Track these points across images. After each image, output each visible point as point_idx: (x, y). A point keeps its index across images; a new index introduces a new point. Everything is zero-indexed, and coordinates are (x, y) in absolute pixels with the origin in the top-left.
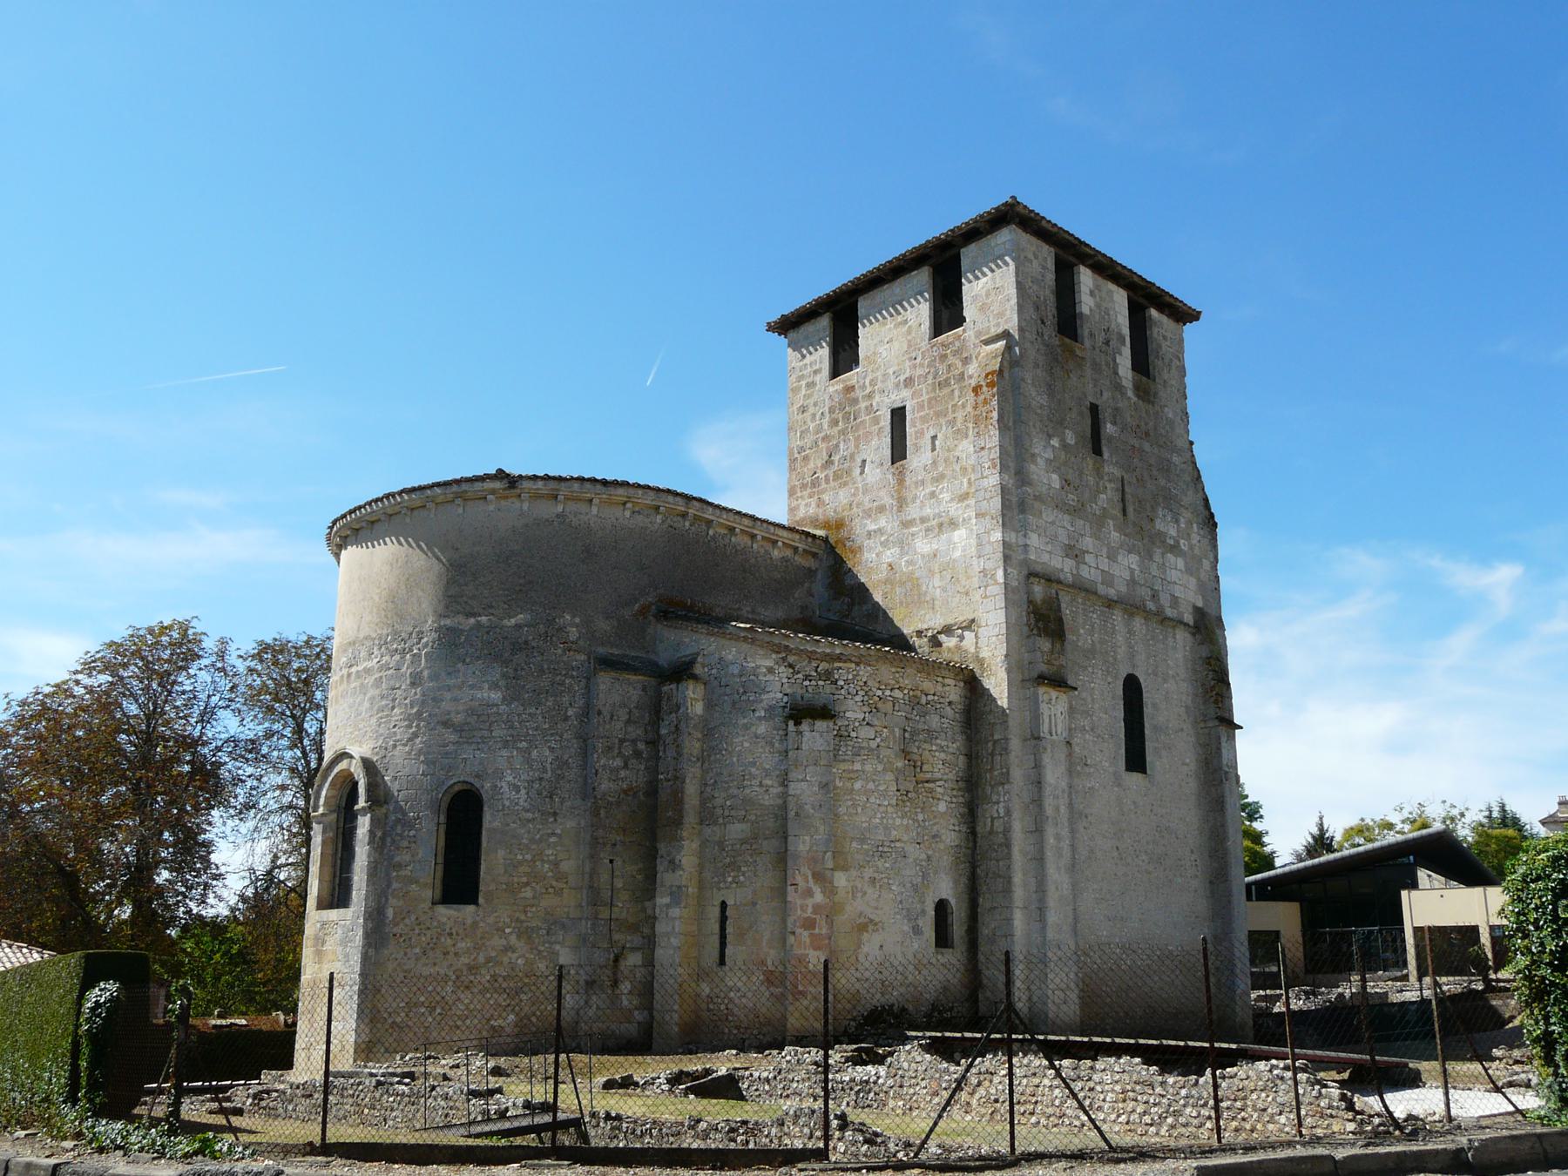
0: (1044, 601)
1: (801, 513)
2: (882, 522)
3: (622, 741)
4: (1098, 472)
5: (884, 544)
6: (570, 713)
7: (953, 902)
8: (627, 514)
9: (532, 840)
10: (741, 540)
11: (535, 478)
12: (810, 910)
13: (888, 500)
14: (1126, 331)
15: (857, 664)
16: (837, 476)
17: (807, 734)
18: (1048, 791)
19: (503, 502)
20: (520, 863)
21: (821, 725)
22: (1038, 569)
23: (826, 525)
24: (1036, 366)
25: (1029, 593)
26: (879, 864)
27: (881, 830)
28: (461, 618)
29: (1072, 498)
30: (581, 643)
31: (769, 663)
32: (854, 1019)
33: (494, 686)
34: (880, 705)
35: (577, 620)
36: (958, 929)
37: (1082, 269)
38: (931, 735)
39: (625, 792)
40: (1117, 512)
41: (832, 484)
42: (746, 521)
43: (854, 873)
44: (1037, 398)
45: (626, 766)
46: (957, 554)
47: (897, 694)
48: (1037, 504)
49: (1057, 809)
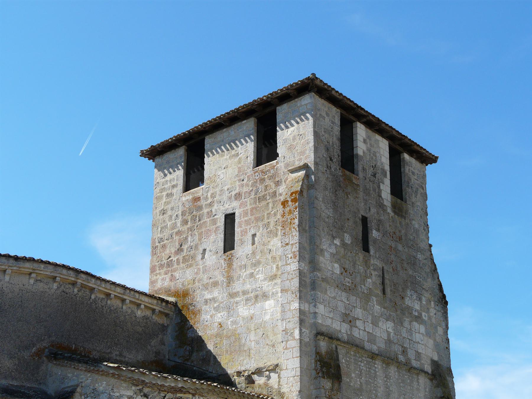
0: (327, 353)
1: (159, 285)
2: (216, 293)
5: (217, 309)
13: (220, 278)
14: (387, 168)
16: (185, 260)
22: (324, 329)
23: (176, 294)
24: (326, 189)
29: (348, 281)
40: (379, 292)
41: (182, 265)
42: (119, 290)
44: (326, 211)
46: (267, 317)
48: (324, 284)
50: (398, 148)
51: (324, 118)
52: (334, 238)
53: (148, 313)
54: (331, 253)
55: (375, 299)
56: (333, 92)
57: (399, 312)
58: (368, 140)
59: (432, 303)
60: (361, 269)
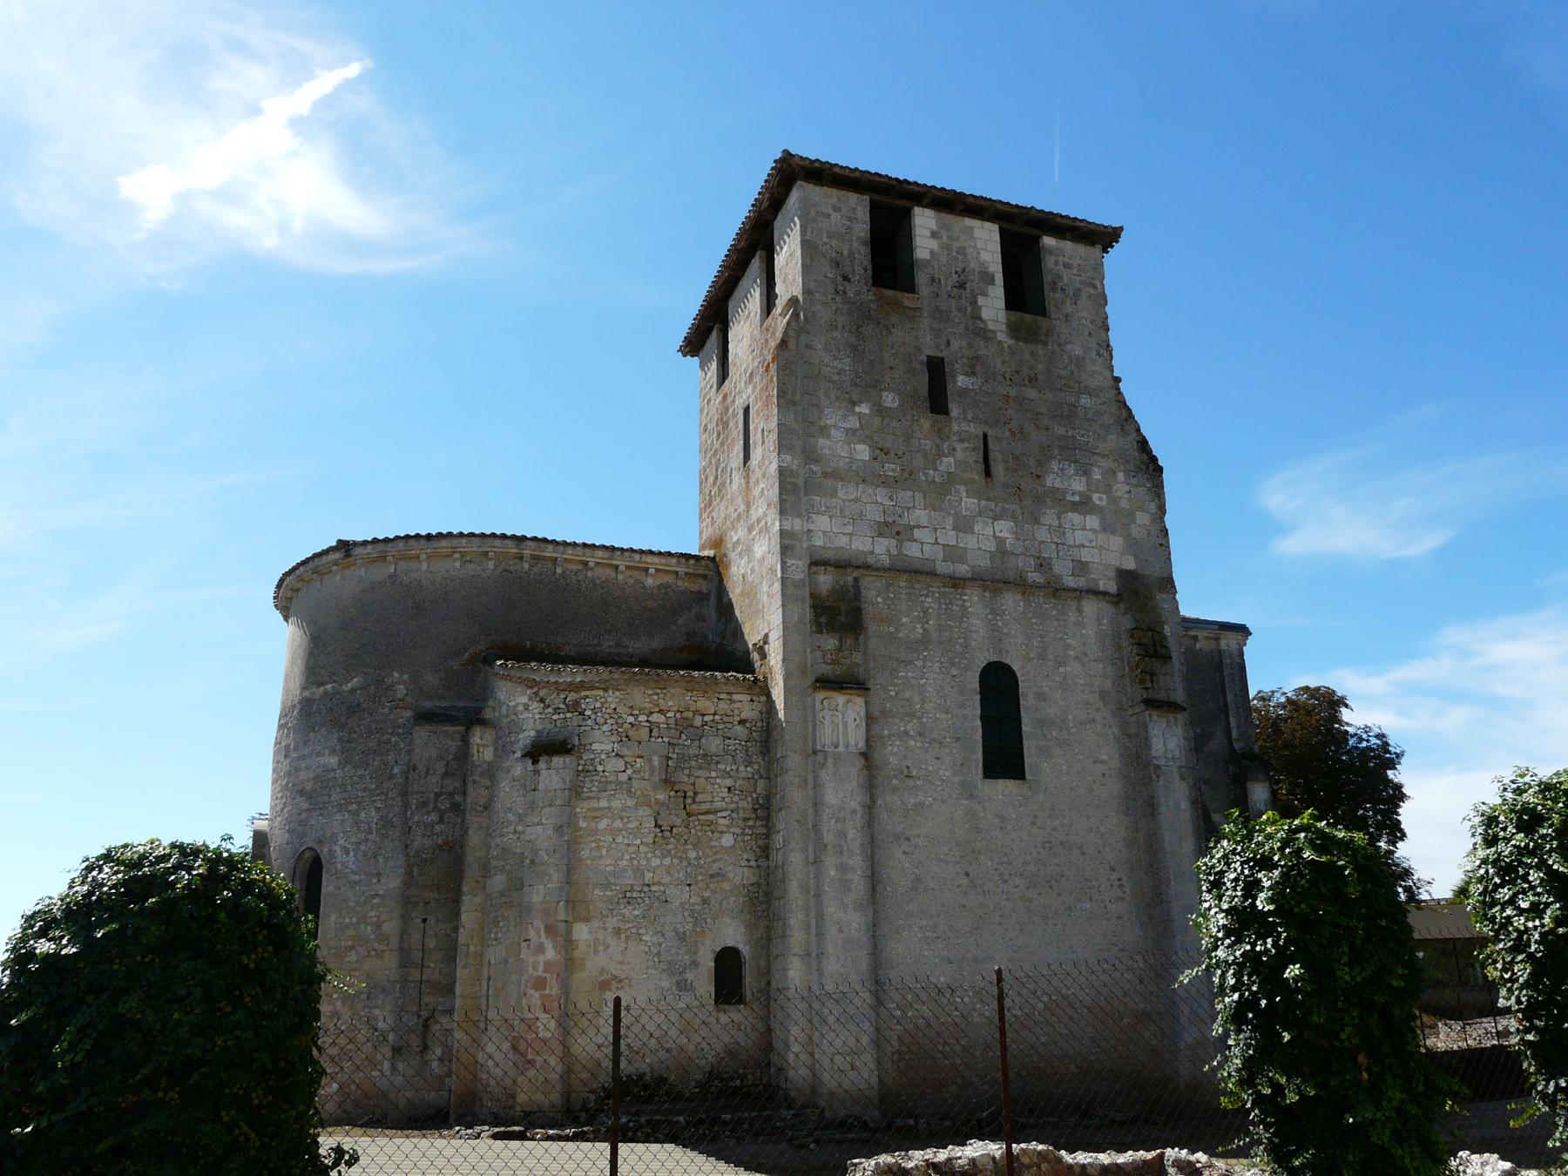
0: (832, 591)
3: (437, 795)
4: (941, 434)
6: (396, 770)
7: (745, 950)
8: (458, 564)
9: (357, 903)
10: (604, 573)
11: (365, 543)
12: (541, 968)
14: (996, 268)
15: (605, 690)
17: (543, 772)
18: (827, 814)
19: (348, 572)
20: (348, 926)
21: (557, 761)
24: (832, 326)
25: (813, 583)
26: (626, 912)
27: (629, 873)
28: (314, 689)
29: (891, 469)
30: (409, 699)
31: (524, 700)
32: (593, 1092)
33: (333, 752)
34: (631, 733)
35: (406, 677)
36: (750, 979)
37: (917, 210)
38: (708, 760)
39: (440, 847)
40: (976, 475)
42: (600, 553)
43: (596, 923)
44: (835, 363)
45: (441, 821)
47: (655, 718)
48: (828, 483)
49: (843, 834)
50: (1027, 230)
51: (829, 216)
52: (854, 404)
53: (668, 579)
54: (847, 430)
55: (962, 488)
56: (836, 170)
57: (1028, 502)
58: (943, 232)
59: (1121, 476)
60: (928, 444)
